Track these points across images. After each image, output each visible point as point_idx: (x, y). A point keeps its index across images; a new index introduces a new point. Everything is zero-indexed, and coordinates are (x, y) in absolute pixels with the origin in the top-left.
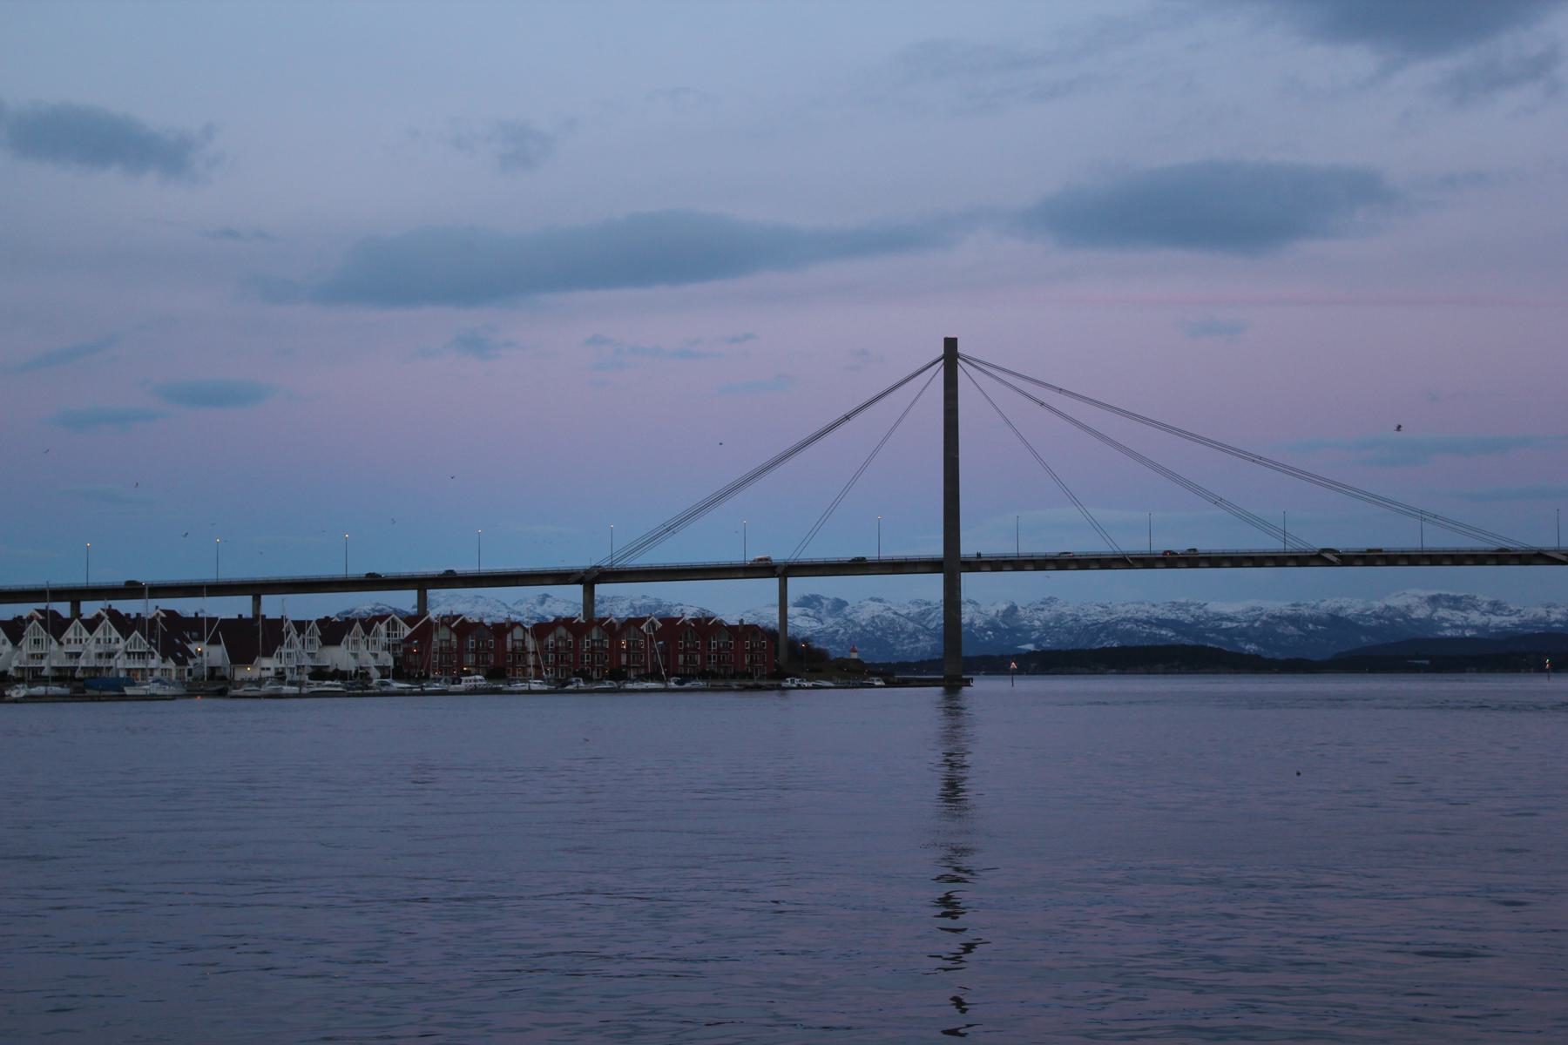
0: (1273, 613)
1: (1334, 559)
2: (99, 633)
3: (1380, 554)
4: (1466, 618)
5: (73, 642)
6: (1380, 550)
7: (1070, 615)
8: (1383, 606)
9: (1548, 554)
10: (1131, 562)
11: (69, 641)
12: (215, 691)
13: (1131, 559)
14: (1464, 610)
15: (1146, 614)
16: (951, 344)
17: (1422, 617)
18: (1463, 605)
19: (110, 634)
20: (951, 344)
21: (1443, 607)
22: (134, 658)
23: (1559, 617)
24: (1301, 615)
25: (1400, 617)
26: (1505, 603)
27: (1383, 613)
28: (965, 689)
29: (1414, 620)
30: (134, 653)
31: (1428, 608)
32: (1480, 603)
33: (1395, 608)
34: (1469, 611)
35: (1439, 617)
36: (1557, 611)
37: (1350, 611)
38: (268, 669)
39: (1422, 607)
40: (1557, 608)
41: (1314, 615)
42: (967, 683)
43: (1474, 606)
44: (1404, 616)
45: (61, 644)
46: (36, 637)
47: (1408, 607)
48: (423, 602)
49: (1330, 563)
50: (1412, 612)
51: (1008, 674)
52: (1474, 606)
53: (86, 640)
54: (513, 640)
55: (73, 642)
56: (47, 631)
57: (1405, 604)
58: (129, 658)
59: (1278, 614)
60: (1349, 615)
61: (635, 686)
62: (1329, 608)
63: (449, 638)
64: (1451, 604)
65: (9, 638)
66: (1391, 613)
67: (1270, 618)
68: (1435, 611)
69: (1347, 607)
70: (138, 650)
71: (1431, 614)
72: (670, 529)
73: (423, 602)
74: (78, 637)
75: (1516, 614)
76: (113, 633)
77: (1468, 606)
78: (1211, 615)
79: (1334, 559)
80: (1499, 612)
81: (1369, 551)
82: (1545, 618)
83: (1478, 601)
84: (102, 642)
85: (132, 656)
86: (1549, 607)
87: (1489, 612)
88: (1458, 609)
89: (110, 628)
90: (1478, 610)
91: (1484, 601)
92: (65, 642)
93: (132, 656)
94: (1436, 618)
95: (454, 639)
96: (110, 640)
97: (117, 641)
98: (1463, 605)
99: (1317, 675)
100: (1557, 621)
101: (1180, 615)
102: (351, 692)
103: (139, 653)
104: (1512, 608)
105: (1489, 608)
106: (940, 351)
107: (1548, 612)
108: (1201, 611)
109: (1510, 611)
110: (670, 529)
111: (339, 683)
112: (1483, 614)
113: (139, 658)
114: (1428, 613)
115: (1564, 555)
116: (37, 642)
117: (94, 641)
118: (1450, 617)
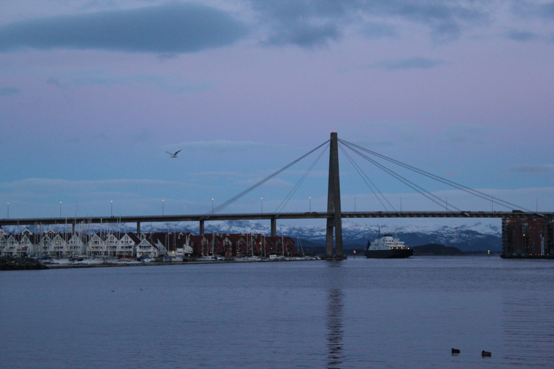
0: (159, 228)
1: (468, 215)
2: (123, 239)
3: (483, 213)
4: (245, 231)
5: (24, 243)
6: (483, 212)
7: (62, 228)
8: (208, 225)
9: (538, 214)
10: (400, 215)
11: (23, 242)
12: (197, 261)
13: (400, 214)
14: (243, 227)
15: (98, 228)
16: (334, 136)
17: (225, 230)
18: (243, 225)
19: (128, 239)
20: (334, 136)
21: (235, 226)
22: (142, 248)
23: (286, 230)
24: (171, 228)
25: (215, 230)
26: (262, 224)
27: (207, 228)
28: (344, 260)
29: (222, 231)
30: (142, 247)
31: (228, 226)
32: (251, 224)
33: (213, 226)
34: (246, 228)
35: (233, 230)
36: (285, 228)
37: (192, 227)
38: (181, 252)
39: (225, 225)
40: (285, 226)
41: (178, 229)
42: (346, 258)
43: (248, 225)
44: (217, 229)
45: (20, 243)
46: (96, 240)
47: (219, 225)
48: (138, 226)
49: (466, 216)
50: (221, 228)
51: (352, 255)
52: (248, 225)
53: (116, 242)
54: (225, 242)
55: (24, 243)
56: (62, 238)
57: (218, 224)
58: (140, 248)
59: (161, 228)
60: (193, 229)
61: (239, 260)
62: (183, 226)
63: (205, 241)
64: (238, 224)
65: (133, 240)
66: (211, 228)
67: (157, 230)
68: (231, 227)
69: (191, 225)
70: (145, 245)
71: (229, 229)
72: (234, 199)
73: (138, 226)
74: (112, 241)
75: (267, 229)
76: (129, 239)
77: (246, 225)
78: (128, 229)
79: (468, 215)
80: (259, 228)
81: (479, 212)
82: (280, 231)
83: (250, 223)
84: (124, 242)
85: (142, 248)
86: (281, 226)
87: (255, 228)
88: (241, 226)
89: (127, 237)
90: (250, 227)
91: (253, 223)
92: (21, 243)
93: (142, 248)
94: (231, 231)
95: (208, 242)
96: (127, 242)
97: (131, 242)
98: (243, 225)
99: (438, 255)
100: (284, 233)
101: (114, 228)
102: (76, 262)
103: (145, 247)
104: (265, 226)
105: (254, 226)
106: (329, 138)
107: (281, 228)
108: (124, 226)
109: (264, 228)
110: (234, 199)
111: (14, 257)
112: (252, 229)
113: (144, 248)
114: (228, 228)
115: (544, 214)
116: (96, 242)
117: (121, 242)
118: (237, 230)
